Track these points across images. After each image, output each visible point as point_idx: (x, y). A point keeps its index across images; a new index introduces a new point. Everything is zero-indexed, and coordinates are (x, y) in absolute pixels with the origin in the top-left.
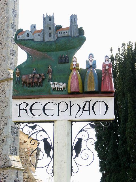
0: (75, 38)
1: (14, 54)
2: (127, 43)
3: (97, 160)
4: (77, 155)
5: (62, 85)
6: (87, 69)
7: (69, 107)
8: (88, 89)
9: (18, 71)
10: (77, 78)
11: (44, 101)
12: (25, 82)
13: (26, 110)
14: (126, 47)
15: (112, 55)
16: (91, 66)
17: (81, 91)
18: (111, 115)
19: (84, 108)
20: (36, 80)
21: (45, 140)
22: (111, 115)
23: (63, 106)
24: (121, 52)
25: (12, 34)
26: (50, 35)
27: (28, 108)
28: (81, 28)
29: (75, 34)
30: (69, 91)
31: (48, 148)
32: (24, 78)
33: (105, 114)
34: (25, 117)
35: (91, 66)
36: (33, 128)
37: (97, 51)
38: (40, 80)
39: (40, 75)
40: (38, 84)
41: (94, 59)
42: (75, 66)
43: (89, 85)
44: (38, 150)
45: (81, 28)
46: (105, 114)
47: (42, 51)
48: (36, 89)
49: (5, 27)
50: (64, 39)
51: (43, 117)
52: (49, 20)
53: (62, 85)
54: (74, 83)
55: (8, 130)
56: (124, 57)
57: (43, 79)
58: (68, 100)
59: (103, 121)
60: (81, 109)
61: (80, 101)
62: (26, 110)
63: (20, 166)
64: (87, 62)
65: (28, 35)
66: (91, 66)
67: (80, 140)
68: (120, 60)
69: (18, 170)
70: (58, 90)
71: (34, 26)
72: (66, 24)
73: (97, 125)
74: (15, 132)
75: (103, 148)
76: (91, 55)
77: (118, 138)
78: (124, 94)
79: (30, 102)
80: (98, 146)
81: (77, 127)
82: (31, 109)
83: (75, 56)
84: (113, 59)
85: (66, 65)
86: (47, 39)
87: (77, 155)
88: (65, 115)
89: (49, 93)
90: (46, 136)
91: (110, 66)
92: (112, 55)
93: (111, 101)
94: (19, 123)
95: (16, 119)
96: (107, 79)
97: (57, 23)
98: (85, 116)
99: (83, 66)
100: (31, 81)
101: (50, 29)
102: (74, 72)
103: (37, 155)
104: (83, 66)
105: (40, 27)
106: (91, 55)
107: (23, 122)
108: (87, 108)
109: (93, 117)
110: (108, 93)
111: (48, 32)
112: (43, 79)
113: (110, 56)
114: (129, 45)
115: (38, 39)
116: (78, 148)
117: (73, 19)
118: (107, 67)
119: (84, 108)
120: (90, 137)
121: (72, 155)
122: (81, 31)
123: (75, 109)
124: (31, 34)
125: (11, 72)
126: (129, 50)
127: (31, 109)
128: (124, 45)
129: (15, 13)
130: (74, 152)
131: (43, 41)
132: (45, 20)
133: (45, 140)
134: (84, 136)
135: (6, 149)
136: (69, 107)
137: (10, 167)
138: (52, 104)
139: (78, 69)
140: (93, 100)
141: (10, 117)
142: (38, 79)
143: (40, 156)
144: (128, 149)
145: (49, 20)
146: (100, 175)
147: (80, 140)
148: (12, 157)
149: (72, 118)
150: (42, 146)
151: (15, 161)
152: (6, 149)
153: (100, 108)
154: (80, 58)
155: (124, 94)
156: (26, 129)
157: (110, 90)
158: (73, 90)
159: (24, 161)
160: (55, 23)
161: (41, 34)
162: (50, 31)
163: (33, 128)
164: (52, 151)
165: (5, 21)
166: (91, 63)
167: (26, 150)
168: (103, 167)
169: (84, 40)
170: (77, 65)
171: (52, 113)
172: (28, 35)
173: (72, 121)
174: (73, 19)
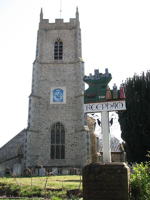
0: (107, 77)
1: (84, 85)
2: (129, 78)
3: (120, 126)
4: (111, 125)
5: (103, 97)
6: (113, 90)
7: (107, 106)
8: (114, 98)
9: (85, 92)
10: (110, 94)
11: (96, 104)
12: (89, 97)
13: (90, 108)
14: (128, 80)
15: (123, 83)
16: (115, 88)
17: (111, 99)
18: (124, 108)
19: (113, 106)
20: (93, 96)
21: (98, 120)
22: (124, 108)
23: (104, 106)
24: (127, 82)
25: (82, 77)
26: (97, 77)
27: (90, 107)
28: (110, 73)
29: (108, 76)
30: (106, 99)
31: (99, 123)
32: (88, 95)
33: (42, 10)
34: (89, 110)
35: (115, 89)
36: (93, 115)
37: (117, 82)
38: (95, 96)
39: (94, 94)
40: (94, 97)
41: (116, 86)
42: (108, 89)
43: (115, 96)
44: (95, 123)
45: (110, 73)
46: (42, 10)
47: (94, 84)
48: (93, 99)
49: (79, 75)
50: (103, 78)
51: (97, 110)
52: (97, 71)
53: (103, 97)
54: (108, 96)
55: (83, 115)
56: (128, 84)
57: (96, 95)
58: (106, 103)
59: (121, 111)
60: (112, 106)
61: (112, 103)
62: (90, 108)
63: (88, 129)
64: (113, 87)
65: (89, 78)
66: (115, 88)
67: (112, 119)
68: (126, 85)
69: (88, 131)
70: (103, 99)
71: (91, 74)
72: (103, 72)
73: (119, 112)
74: (86, 116)
75: (121, 121)
76: (115, 84)
77: (127, 117)
78: (129, 98)
79: (91, 104)
80: (119, 120)
81: (110, 113)
82: (91, 107)
83: (109, 85)
84: (123, 85)
85: (105, 89)
86: (96, 79)
87: (111, 125)
88: (105, 109)
89: (99, 101)
90: (98, 118)
91: (123, 88)
92: (123, 83)
93: (124, 102)
94: (87, 113)
95: (85, 111)
96: (122, 93)
97: (100, 72)
98: (114, 109)
99: (112, 89)
100: (91, 96)
101: (97, 75)
102: (108, 91)
103: (95, 126)
104: (112, 89)
105: (93, 74)
106: (115, 84)
107: (89, 113)
108: (114, 106)
109: (117, 109)
110: (122, 99)
111: (96, 76)
112: (96, 95)
113: (122, 84)
114: (129, 79)
115: (93, 79)
116: (111, 122)
117: (107, 70)
118: (122, 89)
119: (113, 106)
120: (115, 117)
121: (109, 125)
122: (110, 75)
123: (109, 106)
124: (90, 77)
125: (83, 92)
126: (130, 80)
127: (91, 107)
128: (127, 79)
129: (83, 69)
130: (110, 123)
131: (95, 80)
132: (95, 71)
133: (98, 120)
134: (113, 117)
135: (83, 123)
136: (107, 106)
137: (84, 130)
138: (100, 105)
139: (110, 90)
140: (117, 102)
141: (83, 110)
142: (94, 95)
143: (96, 126)
144: (132, 121)
145: (97, 71)
146: (121, 132)
147: (112, 119)
148: (85, 126)
149: (108, 110)
150: (97, 121)
151: (86, 128)
152: (83, 123)
153: (120, 105)
154: (111, 85)
155: (129, 98)
156: (90, 115)
157: (123, 98)
158: (108, 99)
159: (90, 127)
160: (85, 56)
161: (94, 77)
162: (98, 75)
163: (93, 115)
164: (101, 124)
165: (80, 72)
166: (115, 87)
167: (90, 123)
168: (122, 129)
169: (111, 78)
170: (109, 88)
171: (100, 108)
172: (89, 78)
173: (108, 111)
174: (107, 70)
